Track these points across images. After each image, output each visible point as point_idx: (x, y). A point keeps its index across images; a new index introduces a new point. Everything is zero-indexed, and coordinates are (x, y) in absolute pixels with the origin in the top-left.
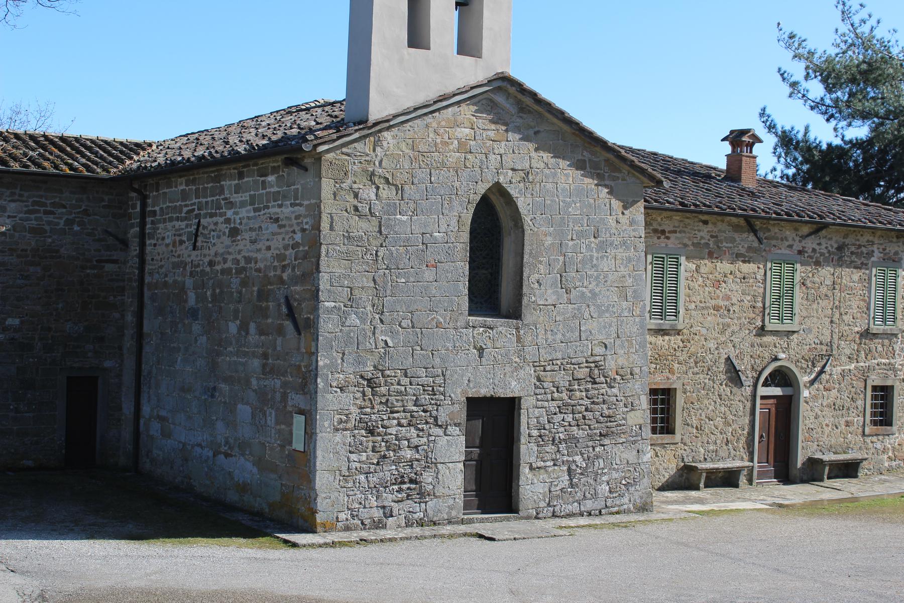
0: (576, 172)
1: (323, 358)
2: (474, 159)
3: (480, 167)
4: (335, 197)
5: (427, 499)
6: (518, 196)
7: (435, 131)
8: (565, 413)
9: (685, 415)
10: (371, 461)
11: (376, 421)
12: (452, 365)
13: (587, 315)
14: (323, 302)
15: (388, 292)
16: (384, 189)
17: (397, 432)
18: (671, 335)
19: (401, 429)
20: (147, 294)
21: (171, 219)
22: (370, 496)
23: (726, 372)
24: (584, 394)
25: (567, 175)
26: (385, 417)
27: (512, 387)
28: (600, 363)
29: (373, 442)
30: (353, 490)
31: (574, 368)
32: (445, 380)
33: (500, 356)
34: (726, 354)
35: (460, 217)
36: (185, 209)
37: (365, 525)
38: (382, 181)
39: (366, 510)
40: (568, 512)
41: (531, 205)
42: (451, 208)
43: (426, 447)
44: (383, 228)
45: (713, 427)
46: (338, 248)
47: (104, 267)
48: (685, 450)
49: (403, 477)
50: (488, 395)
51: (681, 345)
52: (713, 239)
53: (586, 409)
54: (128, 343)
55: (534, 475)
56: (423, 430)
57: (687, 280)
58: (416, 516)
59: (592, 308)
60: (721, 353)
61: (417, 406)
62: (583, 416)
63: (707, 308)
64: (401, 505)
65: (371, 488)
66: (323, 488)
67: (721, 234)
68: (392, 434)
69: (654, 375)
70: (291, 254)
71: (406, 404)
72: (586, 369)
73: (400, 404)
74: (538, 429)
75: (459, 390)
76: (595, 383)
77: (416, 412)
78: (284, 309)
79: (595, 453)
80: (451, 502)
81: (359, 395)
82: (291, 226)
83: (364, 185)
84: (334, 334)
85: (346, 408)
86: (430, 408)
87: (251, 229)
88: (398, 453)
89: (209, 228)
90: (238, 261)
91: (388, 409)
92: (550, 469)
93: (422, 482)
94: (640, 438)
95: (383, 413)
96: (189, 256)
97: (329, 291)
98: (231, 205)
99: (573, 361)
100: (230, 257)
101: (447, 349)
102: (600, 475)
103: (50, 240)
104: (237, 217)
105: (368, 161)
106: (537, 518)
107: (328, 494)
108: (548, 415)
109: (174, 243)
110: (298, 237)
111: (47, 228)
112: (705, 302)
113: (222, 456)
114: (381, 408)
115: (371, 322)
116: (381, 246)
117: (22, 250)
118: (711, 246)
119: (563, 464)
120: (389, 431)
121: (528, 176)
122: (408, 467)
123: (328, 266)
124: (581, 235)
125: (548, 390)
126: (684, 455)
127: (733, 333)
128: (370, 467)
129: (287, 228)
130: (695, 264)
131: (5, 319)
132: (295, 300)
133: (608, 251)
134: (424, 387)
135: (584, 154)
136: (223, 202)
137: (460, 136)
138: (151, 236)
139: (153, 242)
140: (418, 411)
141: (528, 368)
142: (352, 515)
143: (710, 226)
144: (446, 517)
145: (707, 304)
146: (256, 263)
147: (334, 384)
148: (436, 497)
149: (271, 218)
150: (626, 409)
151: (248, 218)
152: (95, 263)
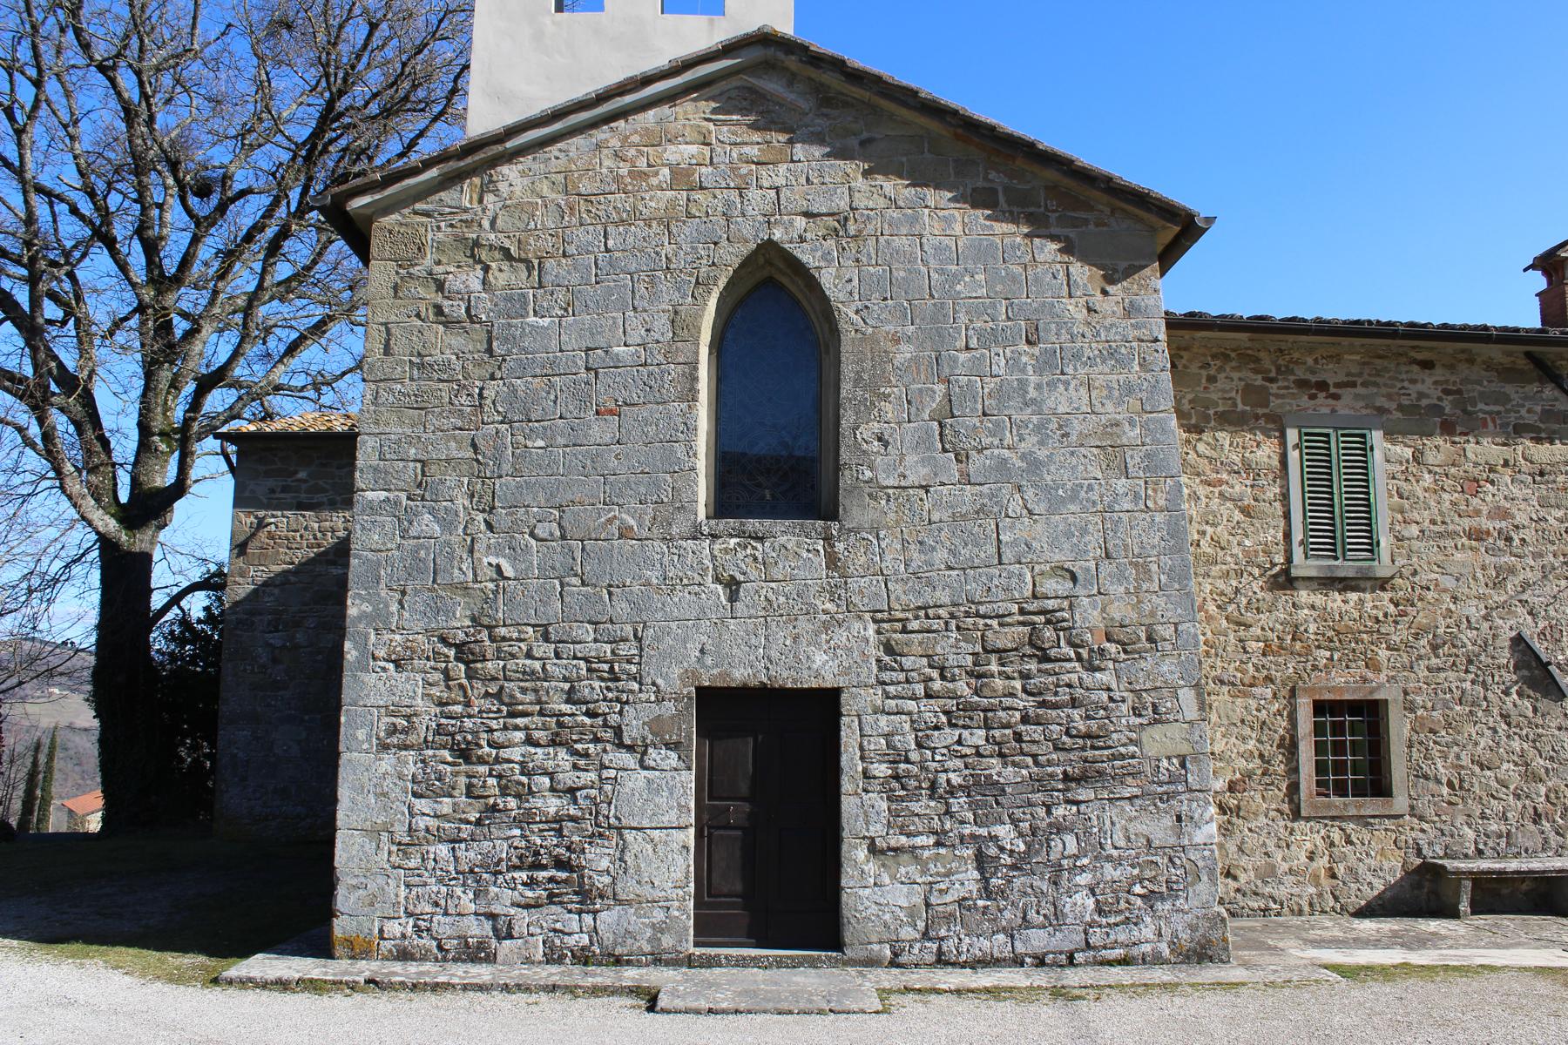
0: (972, 212)
1: (357, 602)
2: (710, 199)
3: (724, 214)
4: (396, 292)
5: (598, 906)
6: (822, 264)
7: (616, 155)
8: (964, 727)
9: (1415, 755)
10: (463, 816)
11: (475, 733)
12: (659, 616)
13: (1015, 507)
14: (363, 490)
15: (507, 468)
16: (501, 270)
17: (523, 756)
18: (1364, 591)
19: (533, 750)
22: (459, 891)
23: (1516, 667)
24: (1018, 684)
25: (948, 221)
26: (494, 725)
27: (815, 666)
28: (1058, 614)
29: (469, 777)
30: (418, 875)
31: (986, 625)
32: (642, 650)
33: (782, 599)
34: (1511, 629)
35: (676, 313)
37: (447, 951)
38: (497, 255)
39: (448, 919)
40: (979, 954)
41: (855, 283)
42: (654, 296)
43: (593, 792)
44: (495, 344)
45: (1494, 784)
46: (399, 386)
48: (1423, 831)
49: (539, 854)
50: (753, 683)
51: (1392, 609)
52: (1450, 398)
53: (1022, 717)
55: (884, 865)
56: (586, 755)
57: (1394, 478)
58: (571, 941)
59: (1030, 494)
60: (1496, 628)
61: (574, 703)
62: (1015, 733)
63: (1452, 535)
64: (535, 915)
65: (463, 873)
66: (350, 865)
67: (1470, 387)
68: (512, 762)
69: (1328, 673)
71: (544, 699)
72: (1021, 628)
73: (530, 697)
74: (891, 762)
75: (676, 671)
76: (1045, 659)
77: (569, 715)
79: (1053, 820)
80: (659, 915)
81: (438, 676)
83: (459, 267)
84: (383, 554)
85: (407, 702)
86: (603, 707)
88: (528, 801)
91: (504, 708)
92: (926, 854)
93: (584, 867)
94: (1180, 788)
95: (491, 715)
97: (376, 469)
99: (982, 609)
101: (648, 584)
102: (1069, 870)
105: (466, 221)
106: (893, 964)
107: (363, 880)
108: (915, 730)
112: (1443, 523)
114: (486, 704)
115: (466, 527)
116: (493, 378)
118: (1447, 410)
119: (962, 842)
120: (505, 753)
121: (845, 225)
122: (552, 833)
123: (377, 423)
124: (991, 338)
125: (913, 674)
126: (1421, 842)
127: (1526, 585)
128: (459, 829)
130: (1410, 447)
133: (1070, 370)
134: (591, 662)
135: (990, 177)
137: (673, 159)
140: (573, 715)
141: (857, 625)
142: (418, 927)
143: (1439, 373)
144: (647, 948)
145: (1451, 527)
147: (381, 653)
148: (620, 902)
150: (1138, 721)
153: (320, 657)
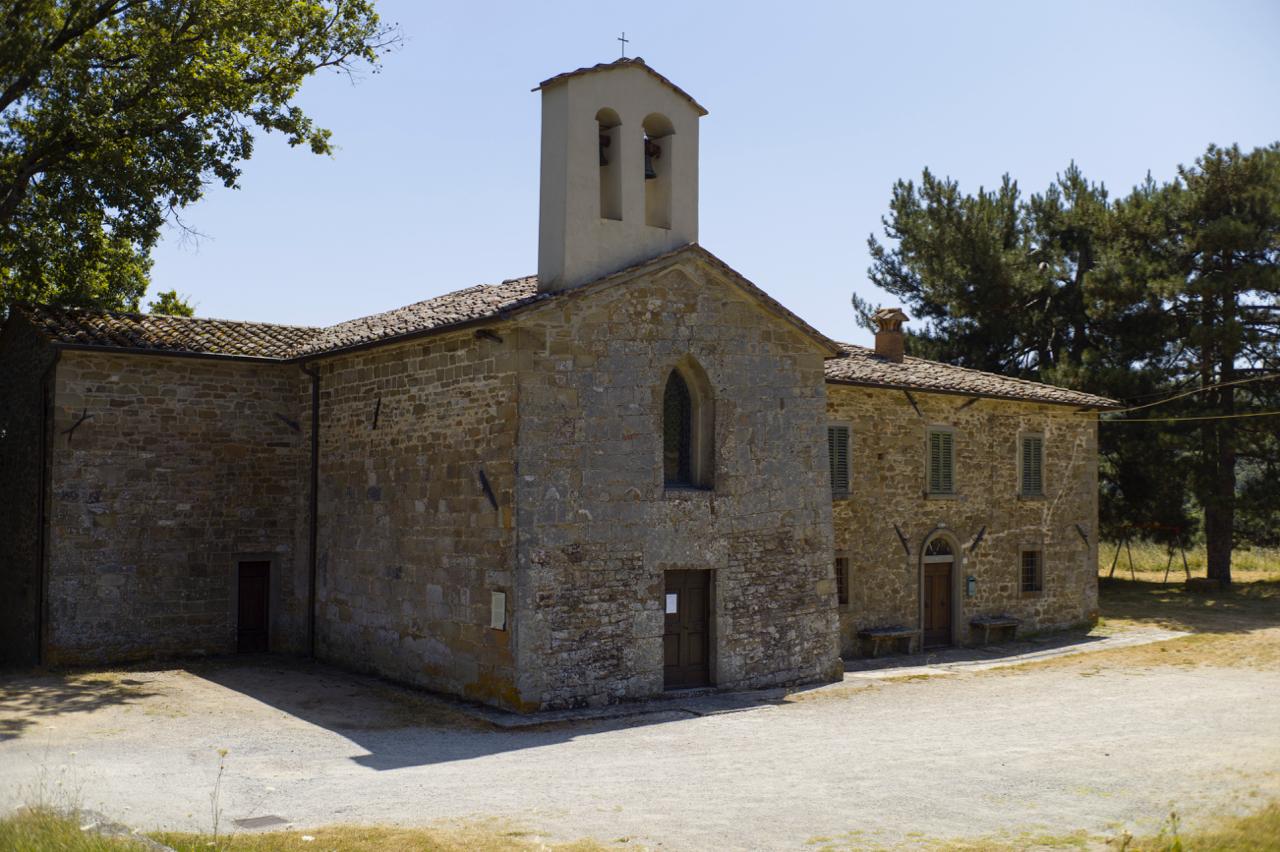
20: (321, 476)
21: (347, 400)
26: (586, 592)
36: (363, 389)
47: (275, 450)
54: (301, 527)
70: (485, 428)
78: (479, 485)
82: (485, 399)
87: (439, 405)
89: (391, 406)
90: (425, 438)
96: (369, 436)
98: (415, 381)
100: (416, 435)
103: (220, 424)
104: (423, 394)
109: (351, 424)
110: (493, 411)
111: (218, 412)
113: (410, 639)
117: (193, 434)
129: (480, 402)
131: (175, 505)
132: (491, 474)
136: (406, 380)
138: (325, 417)
139: (327, 424)
143: (874, 400)
146: (445, 438)
149: (461, 393)
151: (436, 394)
152: (266, 446)
153: (134, 521)
